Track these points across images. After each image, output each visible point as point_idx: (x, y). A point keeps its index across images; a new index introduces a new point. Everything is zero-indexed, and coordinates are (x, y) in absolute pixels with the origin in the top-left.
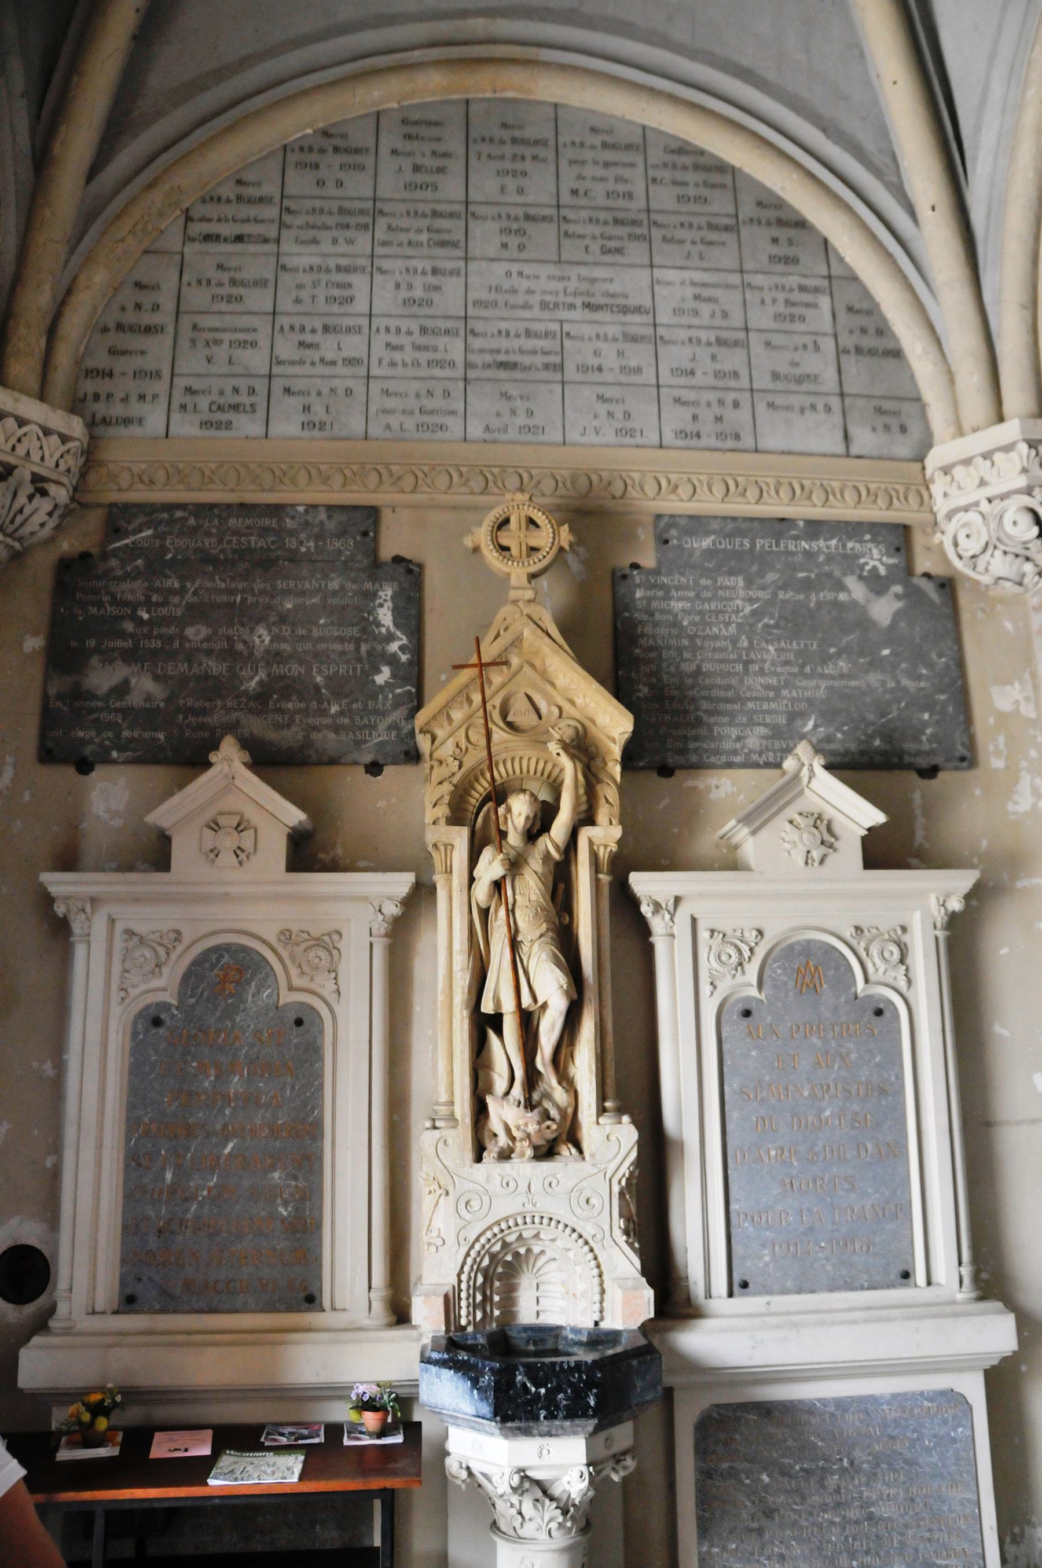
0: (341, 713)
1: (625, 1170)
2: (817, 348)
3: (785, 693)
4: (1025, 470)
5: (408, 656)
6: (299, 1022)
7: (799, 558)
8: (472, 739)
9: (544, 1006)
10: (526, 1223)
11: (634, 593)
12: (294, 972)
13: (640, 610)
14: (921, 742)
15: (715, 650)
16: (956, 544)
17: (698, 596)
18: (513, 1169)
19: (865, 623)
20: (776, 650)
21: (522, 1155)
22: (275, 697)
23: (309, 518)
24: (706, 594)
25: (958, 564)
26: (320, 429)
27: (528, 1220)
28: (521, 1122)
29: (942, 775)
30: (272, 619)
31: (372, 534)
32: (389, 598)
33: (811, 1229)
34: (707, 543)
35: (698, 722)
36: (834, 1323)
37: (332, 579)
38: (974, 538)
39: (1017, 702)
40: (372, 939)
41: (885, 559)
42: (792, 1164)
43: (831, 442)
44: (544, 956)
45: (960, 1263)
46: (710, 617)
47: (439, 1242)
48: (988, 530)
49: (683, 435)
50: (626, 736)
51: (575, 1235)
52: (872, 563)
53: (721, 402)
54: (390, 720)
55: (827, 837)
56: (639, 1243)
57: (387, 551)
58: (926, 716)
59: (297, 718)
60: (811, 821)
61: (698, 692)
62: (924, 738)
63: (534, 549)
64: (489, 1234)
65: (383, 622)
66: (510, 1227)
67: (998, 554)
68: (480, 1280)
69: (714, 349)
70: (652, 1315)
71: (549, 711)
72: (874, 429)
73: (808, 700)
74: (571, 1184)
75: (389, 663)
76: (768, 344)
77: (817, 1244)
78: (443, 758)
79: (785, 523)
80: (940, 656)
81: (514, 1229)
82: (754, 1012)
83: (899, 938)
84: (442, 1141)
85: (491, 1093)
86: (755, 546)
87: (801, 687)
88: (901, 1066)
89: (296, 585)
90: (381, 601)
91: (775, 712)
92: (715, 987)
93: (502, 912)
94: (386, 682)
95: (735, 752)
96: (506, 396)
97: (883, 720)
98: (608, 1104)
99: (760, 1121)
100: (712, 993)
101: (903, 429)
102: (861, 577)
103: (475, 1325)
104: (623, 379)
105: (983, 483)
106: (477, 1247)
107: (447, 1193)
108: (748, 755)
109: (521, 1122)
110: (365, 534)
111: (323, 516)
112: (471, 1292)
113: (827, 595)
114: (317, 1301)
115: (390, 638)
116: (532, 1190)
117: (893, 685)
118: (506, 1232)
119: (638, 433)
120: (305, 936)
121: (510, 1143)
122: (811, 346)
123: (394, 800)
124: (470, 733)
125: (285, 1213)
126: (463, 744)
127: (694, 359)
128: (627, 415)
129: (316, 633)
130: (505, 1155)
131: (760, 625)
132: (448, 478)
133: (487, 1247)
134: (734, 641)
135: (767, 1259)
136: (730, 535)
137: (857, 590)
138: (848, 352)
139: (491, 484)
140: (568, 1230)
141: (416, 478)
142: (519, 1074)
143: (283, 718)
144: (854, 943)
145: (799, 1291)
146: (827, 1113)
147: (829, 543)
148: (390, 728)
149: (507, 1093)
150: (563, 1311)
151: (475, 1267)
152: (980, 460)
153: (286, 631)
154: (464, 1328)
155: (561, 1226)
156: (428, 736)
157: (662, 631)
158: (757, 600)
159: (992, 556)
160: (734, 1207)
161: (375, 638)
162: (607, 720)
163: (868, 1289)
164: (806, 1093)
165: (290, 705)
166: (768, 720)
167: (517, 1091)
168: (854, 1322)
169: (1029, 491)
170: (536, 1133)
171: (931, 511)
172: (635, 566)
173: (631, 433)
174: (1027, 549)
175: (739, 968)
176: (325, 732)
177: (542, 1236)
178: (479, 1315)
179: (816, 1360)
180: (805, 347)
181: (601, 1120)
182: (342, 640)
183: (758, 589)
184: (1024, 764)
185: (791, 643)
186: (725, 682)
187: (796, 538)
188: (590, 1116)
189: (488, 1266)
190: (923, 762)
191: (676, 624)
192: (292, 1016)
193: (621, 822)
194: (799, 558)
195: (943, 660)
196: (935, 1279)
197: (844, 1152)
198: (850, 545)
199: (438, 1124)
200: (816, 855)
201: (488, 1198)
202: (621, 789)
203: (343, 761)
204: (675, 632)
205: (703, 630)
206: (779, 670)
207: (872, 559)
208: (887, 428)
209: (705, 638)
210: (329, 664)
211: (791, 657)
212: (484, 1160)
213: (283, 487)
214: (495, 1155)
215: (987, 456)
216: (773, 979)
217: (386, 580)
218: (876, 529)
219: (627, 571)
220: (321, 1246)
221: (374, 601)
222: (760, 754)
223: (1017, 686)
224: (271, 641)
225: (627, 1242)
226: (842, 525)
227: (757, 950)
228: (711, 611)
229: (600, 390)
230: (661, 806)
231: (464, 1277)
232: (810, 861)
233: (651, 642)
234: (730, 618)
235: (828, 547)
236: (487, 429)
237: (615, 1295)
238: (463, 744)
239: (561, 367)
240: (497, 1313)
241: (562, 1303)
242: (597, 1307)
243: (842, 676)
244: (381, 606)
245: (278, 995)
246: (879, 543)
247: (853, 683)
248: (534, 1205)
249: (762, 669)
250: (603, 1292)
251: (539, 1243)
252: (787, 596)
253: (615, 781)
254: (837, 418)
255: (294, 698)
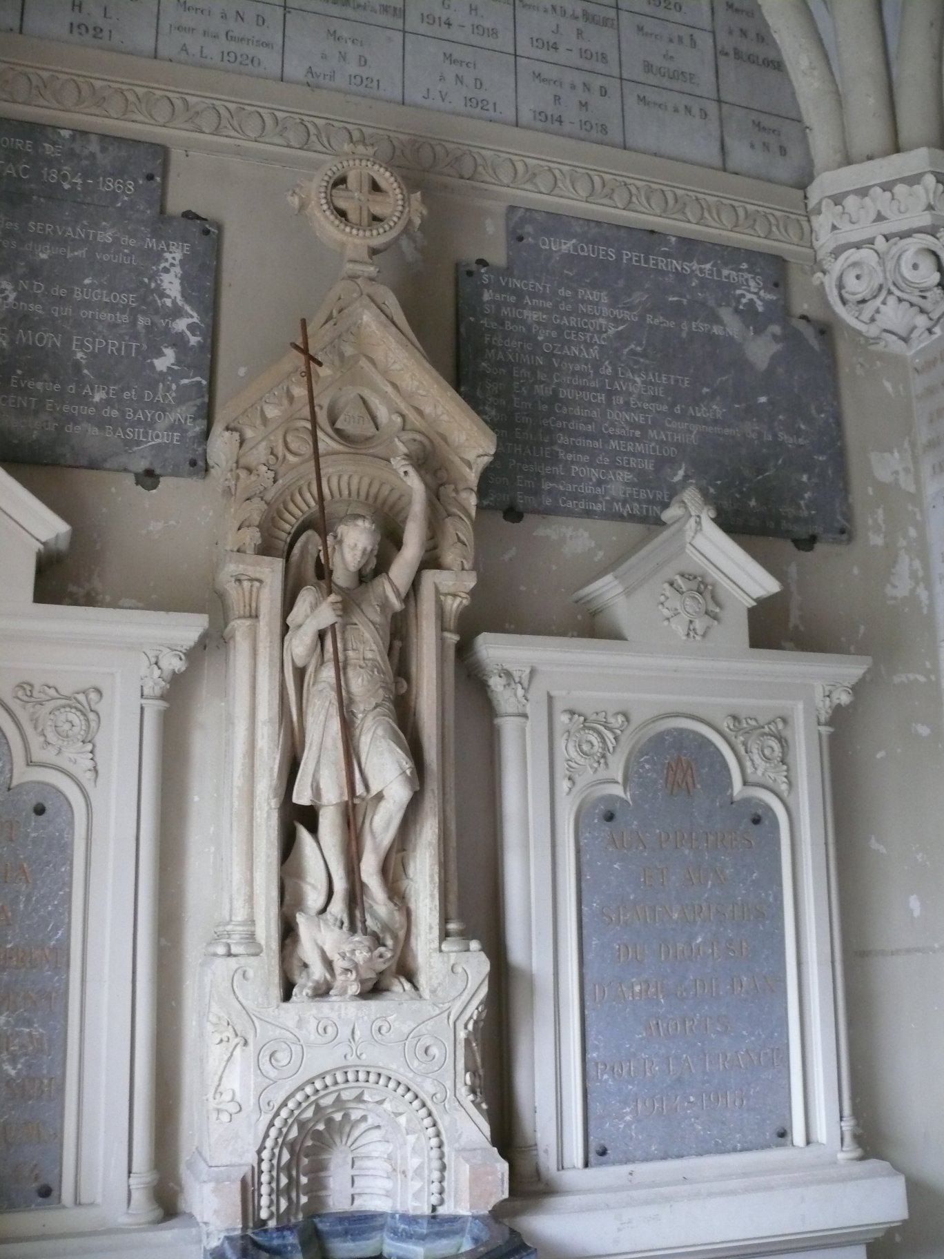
0: (108, 402)
1: (473, 1010)
2: (693, 43)
3: (652, 433)
4: (930, 207)
5: (199, 339)
6: (40, 810)
7: (670, 279)
8: (293, 446)
9: (380, 797)
10: (347, 1081)
11: (482, 295)
12: (35, 741)
13: (487, 315)
14: (799, 507)
15: (574, 373)
16: (840, 286)
17: (556, 306)
18: (332, 1009)
19: (741, 364)
20: (643, 382)
21: (343, 992)
22: (19, 372)
23: (77, 147)
24: (563, 307)
25: (840, 309)
26: (95, 37)
27: (351, 1077)
28: (347, 948)
29: (819, 547)
30: (20, 271)
31: (158, 179)
32: (177, 262)
33: (679, 1080)
34: (567, 246)
35: (554, 459)
36: (710, 1195)
37: (104, 229)
38: (865, 278)
39: (897, 473)
40: (143, 701)
41: (762, 293)
42: (658, 1003)
43: (710, 153)
44: (380, 732)
45: (841, 1118)
46: (569, 334)
47: (233, 1108)
48: (884, 271)
49: (543, 118)
50: (486, 460)
51: (409, 1096)
52: (749, 296)
53: (587, 87)
54: (171, 417)
55: (713, 608)
56: (487, 1104)
57: (177, 203)
58: (805, 478)
59: (49, 403)
60: (694, 585)
61: (554, 422)
62: (802, 503)
63: (376, 219)
64: (299, 1097)
65: (168, 292)
66: (326, 1087)
67: (892, 301)
68: (286, 1156)
69: (580, 24)
70: (506, 1195)
71: (390, 420)
72: (752, 146)
73: (678, 445)
74: (406, 1029)
75: (174, 345)
76: (640, 29)
77: (686, 1099)
78: (253, 464)
79: (656, 236)
80: (820, 411)
81: (332, 1089)
82: (618, 814)
83: (779, 731)
84: (240, 972)
85: (302, 910)
86: (622, 259)
87: (669, 429)
88: (780, 885)
89: (55, 231)
90: (167, 265)
91: (642, 456)
92: (574, 783)
93: (328, 673)
94: (169, 368)
95: (595, 498)
96: (334, 35)
97: (760, 477)
98: (452, 926)
99: (623, 949)
100: (570, 789)
101: (783, 151)
102: (737, 311)
103: (279, 1218)
104: (475, 40)
105: (880, 218)
106: (284, 1113)
107: (246, 1043)
108: (610, 503)
109: (347, 948)
110: (150, 177)
111: (94, 147)
112: (274, 1173)
113: (700, 326)
114: (55, 1194)
115: (177, 313)
116: (357, 1038)
117: (770, 438)
118: (322, 1093)
119: (490, 107)
120: (52, 692)
121: (328, 977)
122: (687, 40)
123: (172, 522)
124: (289, 439)
125: (13, 1073)
126: (280, 450)
127: (557, 31)
128: (479, 83)
129: (78, 296)
130: (322, 992)
131: (625, 351)
132: (259, 121)
133: (296, 1113)
134: (597, 365)
135: (628, 1118)
136: (594, 242)
137: (732, 325)
138: (726, 54)
139: (313, 138)
140: (401, 1090)
141: (220, 117)
142: (340, 885)
143: (29, 402)
144: (731, 735)
145: (665, 1157)
146: (699, 940)
147: (703, 266)
148: (172, 428)
149: (323, 910)
150: (388, 1194)
151: (280, 1140)
152: (878, 190)
153: (39, 287)
154: (264, 1222)
155: (392, 1085)
156: (236, 435)
157: (514, 344)
158: (623, 321)
159: (884, 303)
160: (592, 1055)
161: (157, 312)
162: (463, 437)
163: (741, 1151)
164: (676, 916)
165: (39, 385)
166: (633, 464)
167: (338, 907)
168: (733, 1193)
169: (932, 231)
170: (365, 962)
171: (812, 247)
172: (482, 262)
173: (482, 104)
174: (924, 297)
175: (602, 761)
176: (85, 425)
177: (366, 1097)
178: (284, 1204)
179: (691, 1242)
180: (680, 39)
181: (444, 947)
182: (113, 308)
183: (623, 308)
184: (902, 543)
185: (660, 376)
186: (585, 412)
187: (666, 255)
188: (431, 941)
189: (295, 1139)
190: (802, 532)
191: (529, 338)
192: (31, 800)
193: (475, 568)
194: (670, 279)
195: (823, 416)
196: (813, 1138)
197: (717, 986)
198: (725, 272)
199: (234, 950)
200: (699, 625)
201: (299, 1048)
202: (477, 525)
203: (107, 465)
204: (528, 347)
205: (561, 349)
206: (646, 406)
207: (749, 291)
208: (766, 146)
209: (563, 358)
210: (94, 338)
211: (660, 392)
212: (294, 998)
213: (42, 102)
214: (310, 992)
215: (887, 187)
216: (640, 776)
217: (174, 240)
218: (754, 258)
219: (474, 267)
220: (62, 1116)
221: (157, 263)
222: (624, 502)
223: (896, 455)
224: (17, 299)
225: (473, 1102)
226: (718, 248)
227: (623, 739)
228: (571, 328)
229: (448, 48)
230: (507, 557)
231: (266, 1154)
232: (692, 634)
233: (500, 356)
234: (592, 338)
235: (702, 271)
236: (310, 70)
237: (460, 1172)
238: (280, 450)
239: (402, 13)
240: (304, 1199)
241: (388, 1184)
242: (435, 1187)
243: (716, 422)
244: (166, 270)
245: (11, 770)
246: (758, 274)
247: (727, 431)
248: (359, 1057)
249: (627, 403)
250: (443, 1168)
251: (361, 1106)
252: (656, 321)
253: (469, 516)
254: (713, 125)
255: (46, 376)
